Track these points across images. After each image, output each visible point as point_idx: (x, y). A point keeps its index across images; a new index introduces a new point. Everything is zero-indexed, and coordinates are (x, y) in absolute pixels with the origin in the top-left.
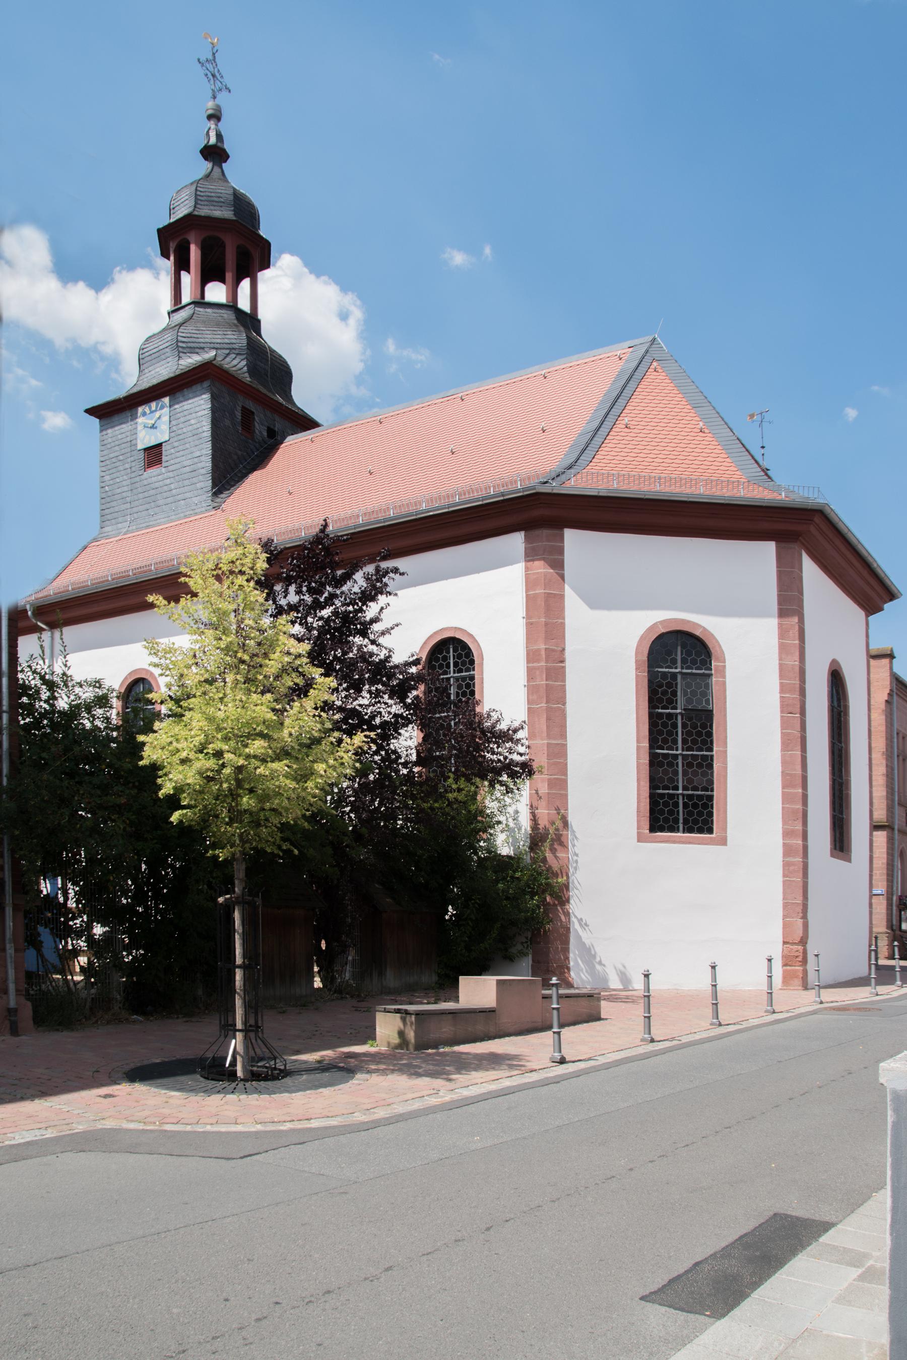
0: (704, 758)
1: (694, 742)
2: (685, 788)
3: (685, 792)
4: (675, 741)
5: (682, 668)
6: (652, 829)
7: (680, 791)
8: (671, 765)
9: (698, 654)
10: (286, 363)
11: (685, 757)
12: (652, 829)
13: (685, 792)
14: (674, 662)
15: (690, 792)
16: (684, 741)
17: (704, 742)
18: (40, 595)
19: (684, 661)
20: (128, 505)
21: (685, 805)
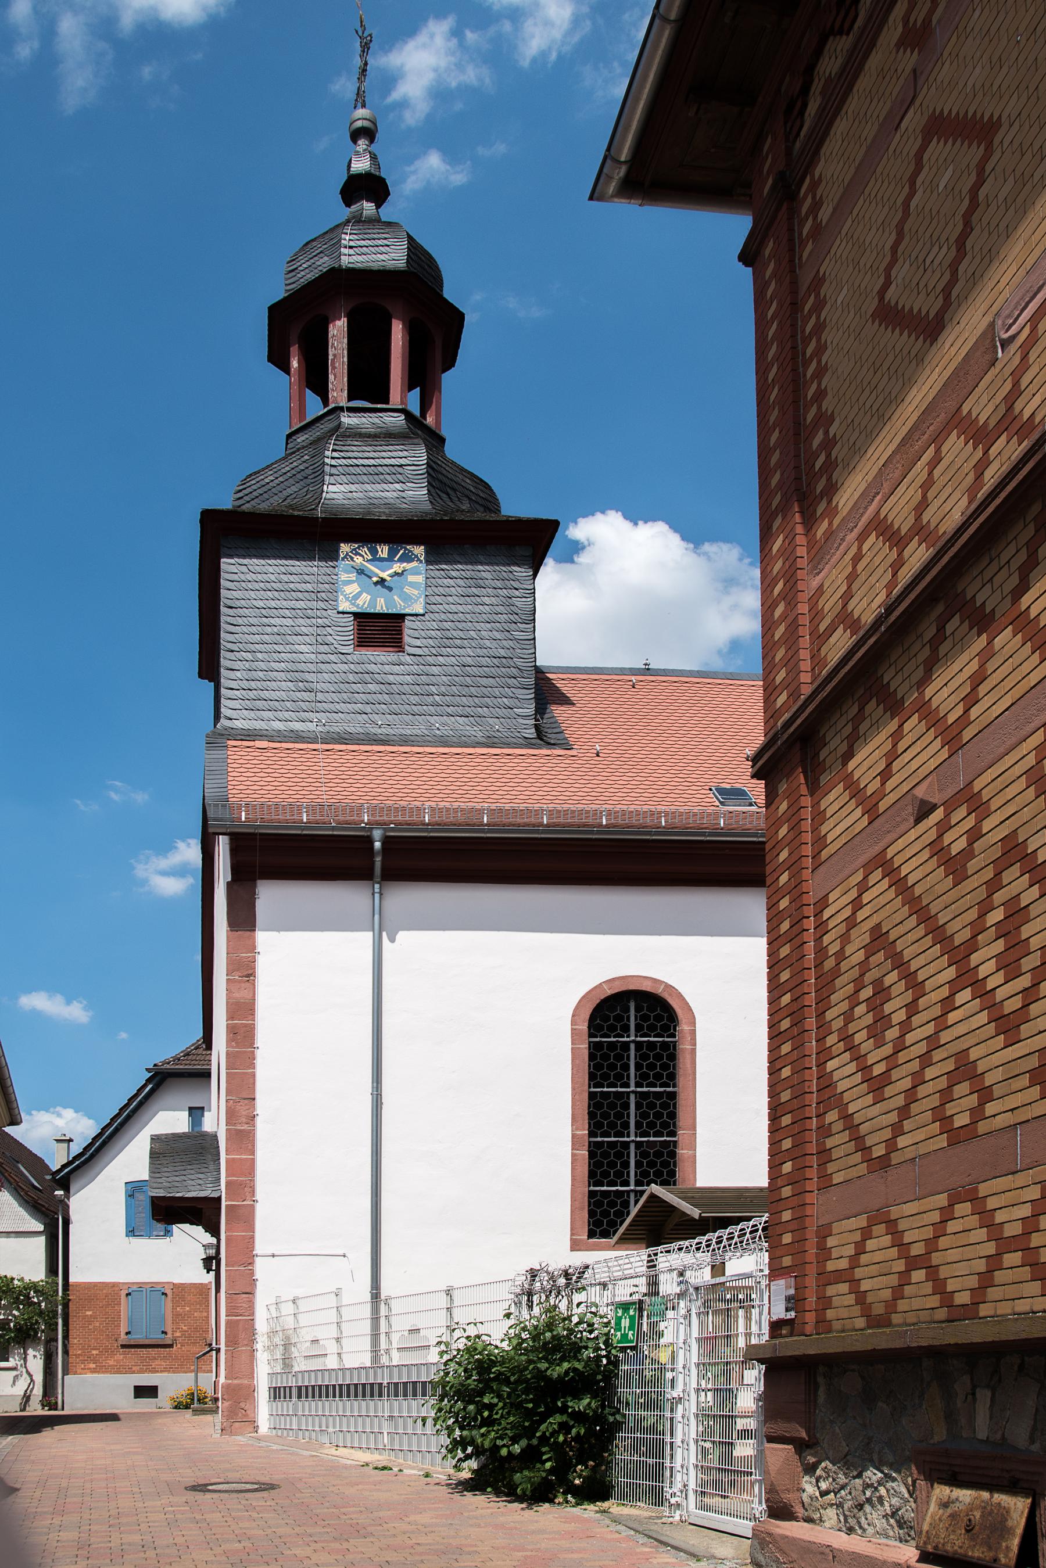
0: (665, 1046)
1: (651, 1125)
2: (638, 1085)
3: (639, 1089)
4: (626, 1125)
5: (636, 1036)
6: (591, 1234)
7: (632, 1088)
8: (619, 1155)
9: (659, 1018)
10: (437, 267)
11: (639, 1045)
12: (591, 1234)
13: (639, 1089)
14: (626, 1029)
15: (645, 1089)
16: (638, 1125)
17: (665, 1125)
18: (351, 266)
19: (638, 1028)
20: (321, 604)
21: (638, 1106)
